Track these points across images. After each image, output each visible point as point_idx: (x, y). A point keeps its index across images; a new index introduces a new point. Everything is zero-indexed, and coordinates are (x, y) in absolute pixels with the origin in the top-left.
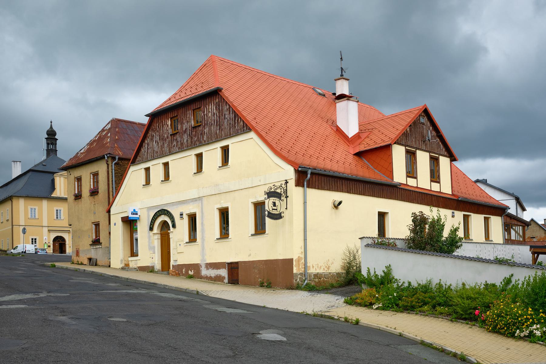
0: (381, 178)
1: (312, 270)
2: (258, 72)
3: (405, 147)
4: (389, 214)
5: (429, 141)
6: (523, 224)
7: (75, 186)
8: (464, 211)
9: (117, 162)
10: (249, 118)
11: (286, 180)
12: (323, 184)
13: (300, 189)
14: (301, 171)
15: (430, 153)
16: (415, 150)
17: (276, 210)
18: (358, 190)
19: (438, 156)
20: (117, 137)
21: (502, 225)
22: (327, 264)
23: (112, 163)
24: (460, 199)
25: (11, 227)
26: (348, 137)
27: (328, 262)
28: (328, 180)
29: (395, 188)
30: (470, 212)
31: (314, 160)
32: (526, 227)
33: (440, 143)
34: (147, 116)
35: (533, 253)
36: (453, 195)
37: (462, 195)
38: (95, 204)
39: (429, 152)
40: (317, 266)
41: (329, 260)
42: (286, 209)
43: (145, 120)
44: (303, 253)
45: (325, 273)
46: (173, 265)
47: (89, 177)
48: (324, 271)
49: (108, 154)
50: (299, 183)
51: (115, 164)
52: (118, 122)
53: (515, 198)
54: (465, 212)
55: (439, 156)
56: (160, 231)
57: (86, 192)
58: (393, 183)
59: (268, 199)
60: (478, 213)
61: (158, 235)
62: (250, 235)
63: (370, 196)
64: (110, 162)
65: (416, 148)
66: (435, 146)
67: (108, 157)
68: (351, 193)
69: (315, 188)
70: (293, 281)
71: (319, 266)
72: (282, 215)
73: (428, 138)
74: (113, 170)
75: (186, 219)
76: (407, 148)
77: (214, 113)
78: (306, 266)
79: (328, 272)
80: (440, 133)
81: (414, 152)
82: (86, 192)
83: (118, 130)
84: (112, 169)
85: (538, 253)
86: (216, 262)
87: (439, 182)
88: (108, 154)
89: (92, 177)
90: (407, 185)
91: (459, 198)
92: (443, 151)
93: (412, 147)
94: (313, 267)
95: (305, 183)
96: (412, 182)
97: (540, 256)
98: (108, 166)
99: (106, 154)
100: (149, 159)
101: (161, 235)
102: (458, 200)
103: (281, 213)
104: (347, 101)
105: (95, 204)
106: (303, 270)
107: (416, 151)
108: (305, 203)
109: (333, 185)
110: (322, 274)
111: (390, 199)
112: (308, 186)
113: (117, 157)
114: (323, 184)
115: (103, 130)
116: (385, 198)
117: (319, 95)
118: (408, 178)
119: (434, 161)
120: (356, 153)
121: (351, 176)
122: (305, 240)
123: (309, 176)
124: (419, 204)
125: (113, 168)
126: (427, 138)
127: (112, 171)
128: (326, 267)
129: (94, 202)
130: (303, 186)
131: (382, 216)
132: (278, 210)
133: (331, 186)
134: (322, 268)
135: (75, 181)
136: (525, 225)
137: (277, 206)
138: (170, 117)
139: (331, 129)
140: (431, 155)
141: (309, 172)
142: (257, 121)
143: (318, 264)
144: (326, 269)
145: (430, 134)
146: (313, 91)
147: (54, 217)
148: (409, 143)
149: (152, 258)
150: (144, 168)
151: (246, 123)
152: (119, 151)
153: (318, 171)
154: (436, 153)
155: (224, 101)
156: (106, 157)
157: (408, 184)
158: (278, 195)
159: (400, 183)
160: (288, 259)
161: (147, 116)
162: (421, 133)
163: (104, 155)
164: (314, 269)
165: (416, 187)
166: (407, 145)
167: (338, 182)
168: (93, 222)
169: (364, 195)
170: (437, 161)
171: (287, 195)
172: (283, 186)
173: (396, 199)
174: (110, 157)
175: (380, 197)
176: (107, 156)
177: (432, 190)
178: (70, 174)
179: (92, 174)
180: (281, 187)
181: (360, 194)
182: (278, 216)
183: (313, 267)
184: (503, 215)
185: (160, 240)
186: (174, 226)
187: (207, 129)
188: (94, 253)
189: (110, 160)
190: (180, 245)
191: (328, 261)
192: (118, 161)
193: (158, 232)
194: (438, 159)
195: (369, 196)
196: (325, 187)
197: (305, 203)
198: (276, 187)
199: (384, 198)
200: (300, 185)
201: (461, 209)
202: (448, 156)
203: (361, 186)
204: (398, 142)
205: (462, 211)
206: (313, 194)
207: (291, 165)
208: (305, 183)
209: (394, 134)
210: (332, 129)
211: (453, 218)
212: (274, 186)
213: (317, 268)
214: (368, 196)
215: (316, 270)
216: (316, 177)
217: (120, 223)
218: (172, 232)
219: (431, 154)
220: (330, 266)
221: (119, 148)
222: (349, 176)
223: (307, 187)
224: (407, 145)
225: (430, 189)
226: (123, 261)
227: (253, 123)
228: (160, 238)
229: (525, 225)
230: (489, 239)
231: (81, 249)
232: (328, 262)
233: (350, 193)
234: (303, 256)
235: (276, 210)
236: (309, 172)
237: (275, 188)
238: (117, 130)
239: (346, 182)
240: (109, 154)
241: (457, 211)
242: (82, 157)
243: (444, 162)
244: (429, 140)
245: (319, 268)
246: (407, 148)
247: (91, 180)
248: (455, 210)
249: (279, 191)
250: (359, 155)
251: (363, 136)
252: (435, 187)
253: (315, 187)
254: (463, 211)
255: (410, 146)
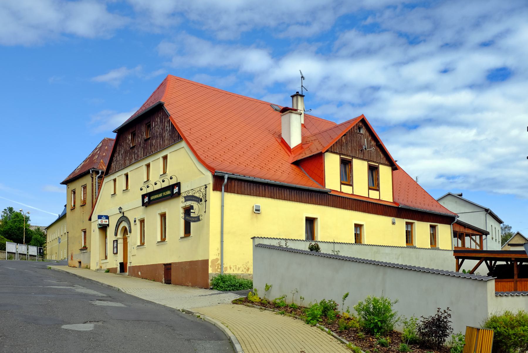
0: (314, 186)
1: (229, 272)
2: (226, 94)
3: (340, 155)
4: (319, 220)
5: (366, 150)
6: (476, 232)
7: (71, 198)
8: (407, 219)
9: (100, 175)
10: (183, 128)
11: (206, 185)
12: (243, 189)
13: (218, 194)
14: (216, 176)
15: (368, 162)
16: (351, 158)
17: (194, 213)
18: (283, 195)
19: (378, 165)
20: (104, 154)
21: (451, 233)
22: (247, 266)
23: (96, 176)
24: (400, 207)
25: (67, 239)
26: (290, 148)
27: (248, 264)
28: (295, 193)
29: (326, 195)
30: (414, 220)
31: (279, 173)
32: (484, 237)
33: (380, 153)
34: (115, 132)
35: (457, 258)
36: (394, 202)
37: (403, 203)
38: (83, 213)
39: (368, 161)
40: (235, 267)
41: (248, 261)
42: (205, 212)
43: (114, 136)
44: (220, 255)
45: (245, 275)
46: (129, 267)
47: (80, 190)
48: (243, 273)
49: (92, 168)
50: (217, 188)
51: (98, 177)
52: (109, 141)
53: (484, 210)
54: (408, 220)
55: (379, 164)
56: (122, 235)
57: (78, 203)
58: (325, 189)
59: (185, 202)
60: (412, 218)
61: (121, 240)
62: (180, 238)
63: (297, 201)
64: (94, 176)
65: (352, 156)
66: (374, 155)
67: (93, 171)
68: (275, 198)
69: (234, 193)
70: (209, 281)
71: (237, 268)
72: (200, 218)
73: (365, 147)
74: (97, 183)
75: (138, 223)
76: (341, 156)
77: (168, 120)
78: (222, 266)
79: (247, 273)
80: (379, 142)
81: (350, 160)
82: (78, 203)
83: (107, 148)
84: (96, 182)
85: (464, 258)
86: (156, 263)
87: (378, 190)
88: (92, 168)
89: (82, 190)
90: (341, 192)
91: (399, 205)
92: (384, 160)
93: (347, 156)
94: (230, 268)
95: (223, 188)
96: (347, 190)
97: (466, 261)
98: (93, 179)
99: (91, 169)
100: (117, 171)
101: (123, 239)
102: (398, 208)
103: (199, 216)
104: (289, 113)
105: (83, 213)
106: (219, 270)
107: (379, 166)
108: (222, 206)
109: (254, 190)
110: (241, 275)
111: (320, 204)
112: (227, 191)
113: (100, 171)
114: (243, 189)
115: (96, 149)
116: (314, 204)
117: (275, 110)
118: (370, 190)
119: (373, 170)
120: (294, 162)
121: (274, 181)
122: (222, 242)
123: (226, 180)
124: (353, 210)
125: (97, 181)
126: (364, 147)
127: (96, 183)
128: (245, 268)
129: (83, 211)
130: (221, 190)
131: (358, 227)
132: (196, 213)
133: (252, 191)
134: (241, 269)
135: (72, 193)
136: (482, 234)
137: (195, 209)
138: (130, 132)
139: (275, 141)
140: (369, 164)
141: (226, 177)
142: (206, 135)
143: (236, 265)
144: (245, 270)
145: (365, 141)
146: (270, 107)
147: (156, 238)
148: (344, 152)
149: (116, 261)
150: (113, 180)
151: (179, 132)
152: (104, 165)
153: (236, 176)
154: (375, 162)
155: (166, 115)
156: (91, 171)
157: (342, 191)
158: (199, 200)
159: (330, 190)
160: (205, 260)
161: (115, 132)
162: (359, 142)
163: (89, 170)
164: (232, 270)
165: (351, 194)
166: (342, 154)
167: (303, 194)
168: (82, 229)
169: (290, 200)
170: (377, 169)
171: (206, 199)
172: (202, 190)
173: (326, 205)
174: (95, 171)
175: (309, 203)
176: (91, 170)
177: (370, 197)
178: (69, 188)
179: (83, 187)
180: (200, 192)
181: (285, 199)
182: (196, 219)
183: (230, 268)
184: (451, 223)
185: (123, 244)
186: (130, 232)
187: (154, 141)
188: (82, 258)
189: (94, 174)
190: (134, 248)
191: (247, 263)
192: (101, 175)
193: (120, 237)
194: (378, 168)
195: (295, 201)
196: (246, 191)
197: (222, 206)
198: (194, 191)
199: (313, 204)
200: (391, 215)
201: (402, 217)
202: (389, 165)
203: (287, 192)
204: (331, 150)
205: (404, 219)
206: (232, 199)
207: (210, 171)
208: (223, 188)
209: (328, 143)
210: (277, 140)
211: (393, 225)
212: (193, 190)
213: (235, 270)
214: (294, 201)
215: (234, 271)
216: (239, 183)
217: (97, 230)
218: (129, 236)
219: (369, 163)
220: (249, 267)
221: (104, 163)
222: (272, 181)
223: (225, 191)
224: (342, 154)
225: (368, 197)
226: (98, 263)
227: (186, 134)
228: (122, 242)
229: (482, 234)
230: (436, 246)
231: (74, 254)
232: (247, 264)
233: (274, 198)
234: (219, 257)
235: (194, 213)
236: (226, 177)
237: (193, 192)
238: (106, 148)
239: (269, 188)
240: (93, 168)
241: (398, 219)
242: (78, 173)
243: (385, 172)
244: (365, 148)
245: (237, 270)
246: (341, 156)
247: (81, 193)
248: (439, 223)
249: (197, 195)
250: (297, 163)
251: (305, 147)
252: (374, 195)
253: (233, 191)
254: (405, 219)
255: (345, 155)
